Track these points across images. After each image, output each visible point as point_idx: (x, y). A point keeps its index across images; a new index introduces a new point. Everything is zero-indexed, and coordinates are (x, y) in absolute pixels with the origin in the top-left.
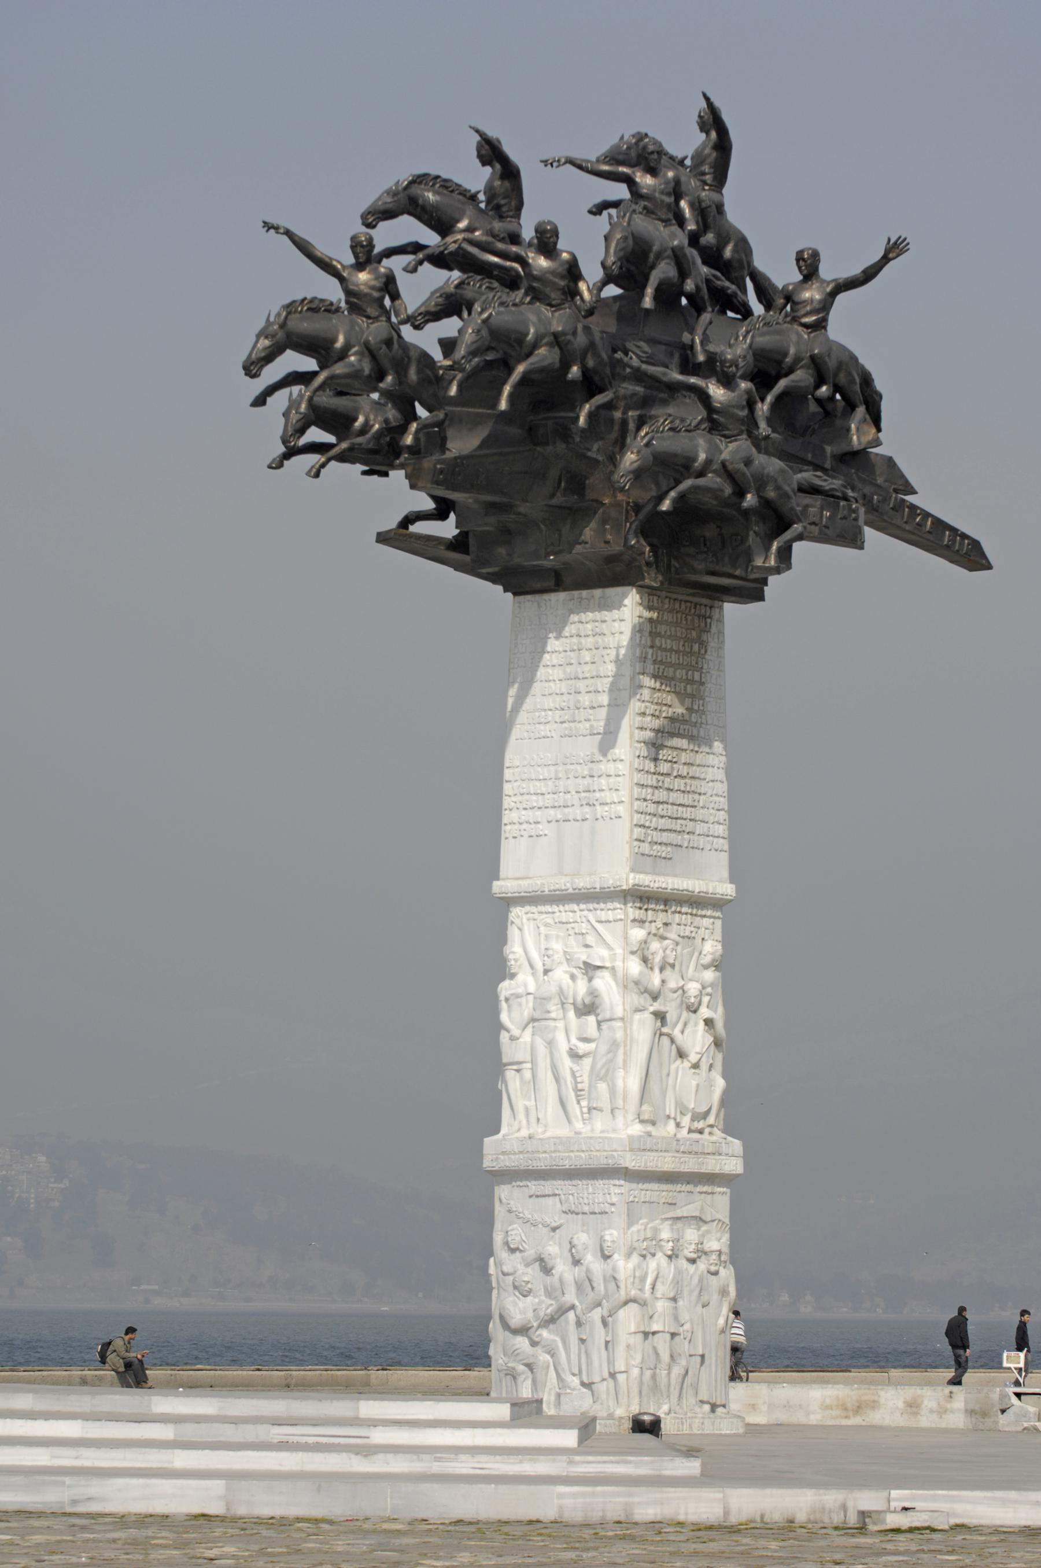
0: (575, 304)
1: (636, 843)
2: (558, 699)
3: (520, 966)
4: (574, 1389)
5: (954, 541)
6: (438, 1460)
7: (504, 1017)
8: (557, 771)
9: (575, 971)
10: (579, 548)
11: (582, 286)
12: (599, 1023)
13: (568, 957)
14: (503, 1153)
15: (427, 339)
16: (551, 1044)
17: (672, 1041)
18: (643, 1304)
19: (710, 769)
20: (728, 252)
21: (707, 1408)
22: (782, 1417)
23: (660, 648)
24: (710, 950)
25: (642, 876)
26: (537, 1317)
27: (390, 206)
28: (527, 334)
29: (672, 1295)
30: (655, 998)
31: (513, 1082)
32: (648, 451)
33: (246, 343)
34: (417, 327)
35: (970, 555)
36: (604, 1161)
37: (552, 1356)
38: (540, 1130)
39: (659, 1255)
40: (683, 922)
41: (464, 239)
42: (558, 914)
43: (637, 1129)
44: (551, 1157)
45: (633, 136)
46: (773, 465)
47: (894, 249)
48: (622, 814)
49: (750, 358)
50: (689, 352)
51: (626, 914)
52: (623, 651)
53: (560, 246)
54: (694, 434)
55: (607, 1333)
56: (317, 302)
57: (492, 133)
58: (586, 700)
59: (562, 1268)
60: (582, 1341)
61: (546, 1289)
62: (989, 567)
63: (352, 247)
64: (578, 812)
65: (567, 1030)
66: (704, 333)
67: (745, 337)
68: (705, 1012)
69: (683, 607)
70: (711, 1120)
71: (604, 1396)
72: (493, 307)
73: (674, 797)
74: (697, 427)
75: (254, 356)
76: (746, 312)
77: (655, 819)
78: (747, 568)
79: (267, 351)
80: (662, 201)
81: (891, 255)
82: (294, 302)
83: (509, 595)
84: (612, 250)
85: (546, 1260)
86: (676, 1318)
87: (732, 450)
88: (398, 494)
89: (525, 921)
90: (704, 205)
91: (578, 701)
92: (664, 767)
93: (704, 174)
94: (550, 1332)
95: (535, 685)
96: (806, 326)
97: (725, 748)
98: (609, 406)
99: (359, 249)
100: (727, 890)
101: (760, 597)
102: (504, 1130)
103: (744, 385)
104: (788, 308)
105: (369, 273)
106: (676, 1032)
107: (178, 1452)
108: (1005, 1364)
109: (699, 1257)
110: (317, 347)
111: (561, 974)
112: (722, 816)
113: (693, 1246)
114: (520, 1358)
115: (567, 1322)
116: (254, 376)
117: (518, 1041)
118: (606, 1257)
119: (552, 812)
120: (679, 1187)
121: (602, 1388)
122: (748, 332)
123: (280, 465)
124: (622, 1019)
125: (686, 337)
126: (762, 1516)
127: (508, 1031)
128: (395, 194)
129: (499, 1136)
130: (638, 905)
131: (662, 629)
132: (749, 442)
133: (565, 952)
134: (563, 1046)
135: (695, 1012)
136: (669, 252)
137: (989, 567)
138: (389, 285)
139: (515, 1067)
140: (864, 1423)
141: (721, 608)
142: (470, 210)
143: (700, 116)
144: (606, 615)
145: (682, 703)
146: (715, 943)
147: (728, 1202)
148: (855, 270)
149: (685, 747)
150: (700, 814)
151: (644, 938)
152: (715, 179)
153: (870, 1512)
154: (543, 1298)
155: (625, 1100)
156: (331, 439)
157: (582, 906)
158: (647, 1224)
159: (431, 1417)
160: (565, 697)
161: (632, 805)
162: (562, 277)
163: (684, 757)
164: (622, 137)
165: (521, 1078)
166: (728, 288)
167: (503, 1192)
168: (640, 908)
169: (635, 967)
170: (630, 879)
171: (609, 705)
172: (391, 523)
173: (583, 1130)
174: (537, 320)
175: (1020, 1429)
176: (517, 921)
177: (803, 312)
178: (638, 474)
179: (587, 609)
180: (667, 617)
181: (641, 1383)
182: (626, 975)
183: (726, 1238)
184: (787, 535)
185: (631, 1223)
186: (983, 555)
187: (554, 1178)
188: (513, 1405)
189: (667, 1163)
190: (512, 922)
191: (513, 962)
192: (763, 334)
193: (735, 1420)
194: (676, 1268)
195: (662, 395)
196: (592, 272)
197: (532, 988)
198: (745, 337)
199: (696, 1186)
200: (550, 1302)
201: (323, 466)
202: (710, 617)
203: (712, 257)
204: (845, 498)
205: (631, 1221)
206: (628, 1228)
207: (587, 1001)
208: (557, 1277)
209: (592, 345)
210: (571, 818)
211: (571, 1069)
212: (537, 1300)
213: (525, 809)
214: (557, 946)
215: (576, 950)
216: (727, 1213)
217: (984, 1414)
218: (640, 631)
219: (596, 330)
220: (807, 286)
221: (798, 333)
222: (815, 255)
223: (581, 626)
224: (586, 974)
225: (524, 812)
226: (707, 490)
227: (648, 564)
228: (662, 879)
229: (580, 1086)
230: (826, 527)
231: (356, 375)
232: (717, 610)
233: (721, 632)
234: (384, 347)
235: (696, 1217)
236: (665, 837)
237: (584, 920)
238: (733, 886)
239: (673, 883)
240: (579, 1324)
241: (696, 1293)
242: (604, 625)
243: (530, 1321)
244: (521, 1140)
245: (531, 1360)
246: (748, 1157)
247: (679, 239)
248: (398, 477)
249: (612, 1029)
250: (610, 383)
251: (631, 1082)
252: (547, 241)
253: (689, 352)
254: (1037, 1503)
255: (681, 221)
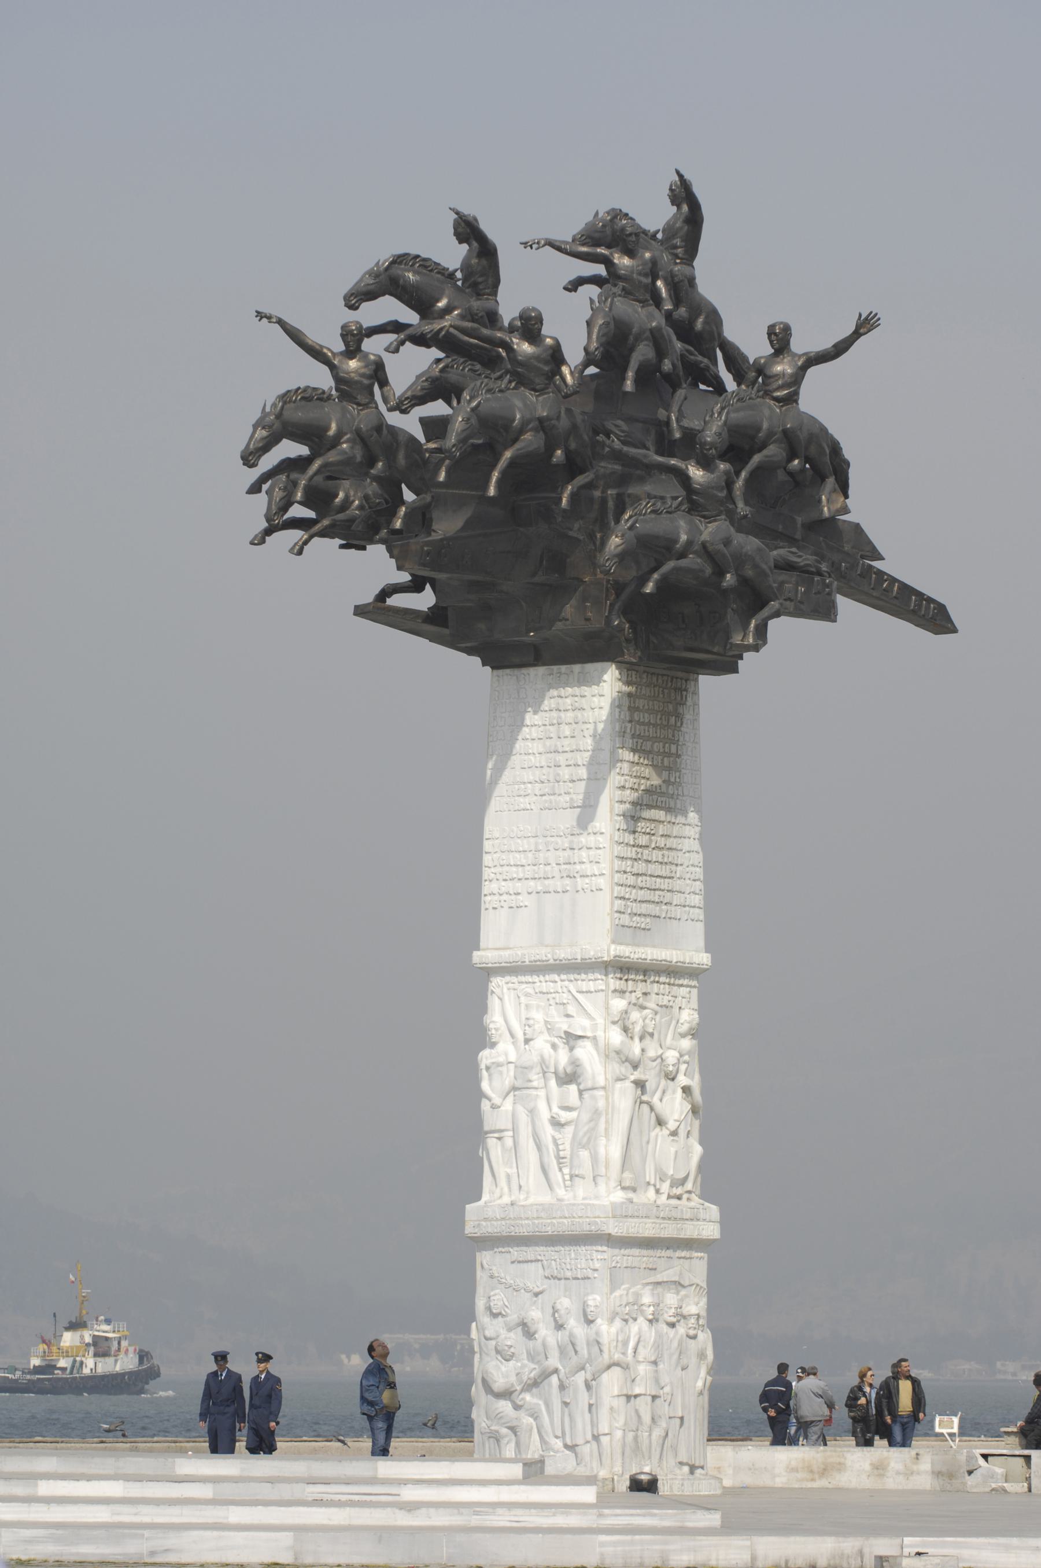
0: (555, 384)
1: (617, 915)
2: (537, 772)
3: (500, 1036)
4: (557, 1452)
5: (920, 606)
6: (476, 1513)
7: (485, 1086)
8: (536, 844)
9: (556, 1040)
10: (559, 625)
11: (565, 370)
12: (581, 1093)
13: (549, 1027)
14: (486, 1219)
15: (410, 423)
16: (532, 1112)
17: (652, 1109)
18: (625, 1367)
19: (687, 840)
20: (699, 324)
21: (686, 1469)
22: (748, 1480)
23: (639, 722)
24: (687, 1018)
25: (622, 947)
26: (520, 1382)
27: (372, 287)
28: (514, 420)
29: (653, 1359)
30: (635, 1067)
31: (495, 1150)
32: (632, 534)
33: (242, 435)
34: (404, 412)
35: (934, 617)
36: (586, 1228)
37: (535, 1419)
38: (522, 1197)
39: (641, 1319)
40: (661, 991)
41: (451, 326)
42: (538, 984)
43: (619, 1196)
44: (533, 1223)
45: (608, 213)
46: (751, 544)
47: (865, 325)
48: (603, 887)
49: (725, 435)
50: (665, 429)
51: (607, 985)
52: (601, 726)
53: (544, 331)
54: (675, 515)
55: (590, 1396)
56: (309, 391)
57: (467, 210)
58: (565, 773)
59: (545, 1332)
60: (566, 1404)
61: (529, 1353)
62: (954, 630)
63: (342, 335)
64: (558, 884)
65: (548, 1099)
66: (680, 410)
67: (720, 414)
68: (682, 1080)
69: (660, 681)
70: (689, 1186)
71: (587, 1458)
72: (481, 395)
73: (653, 869)
74: (677, 508)
75: (251, 446)
76: (719, 388)
77: (634, 891)
78: (725, 646)
79: (265, 442)
80: (640, 282)
81: (862, 331)
82: (289, 391)
83: (488, 669)
84: (594, 337)
85: (529, 1324)
86: (657, 1381)
87: (710, 531)
88: (376, 566)
89: (505, 990)
90: (676, 279)
91: (558, 775)
92: (643, 840)
93: (676, 247)
94: (532, 1396)
95: (513, 758)
96: (777, 400)
97: (701, 819)
98: (590, 486)
99: (349, 338)
100: (703, 959)
101: (735, 670)
102: (485, 1197)
103: (722, 466)
104: (760, 380)
105: (359, 360)
106: (655, 1100)
107: (232, 1508)
108: (938, 1430)
109: (679, 1321)
110: (312, 435)
111: (542, 1044)
112: (698, 886)
113: (673, 1310)
114: (503, 1421)
115: (550, 1385)
116: (251, 466)
117: (499, 1109)
118: (589, 1322)
119: (532, 883)
120: (659, 1253)
121: (585, 1450)
122: (722, 409)
123: (262, 541)
124: (604, 1088)
125: (662, 414)
126: (787, 1562)
127: (490, 1099)
128: (377, 275)
129: (481, 1203)
130: (619, 976)
131: (640, 703)
132: (727, 523)
133: (546, 1022)
134: (544, 1114)
135: (673, 1079)
136: (648, 334)
137: (954, 630)
138: (378, 373)
139: (496, 1135)
140: (830, 1486)
141: (696, 680)
142: (448, 290)
143: (671, 189)
144: (586, 690)
145: (659, 775)
146: (692, 1012)
147: (706, 1266)
148: (825, 343)
149: (662, 819)
150: (677, 884)
151: (625, 1008)
152: (686, 252)
153: (887, 1557)
154: (526, 1362)
155: (607, 1167)
156: (311, 514)
157: (563, 977)
158: (629, 1289)
159: (446, 1476)
160: (545, 770)
161: (613, 877)
162: (546, 363)
163: (661, 829)
164: (597, 214)
165: (503, 1146)
166: (701, 362)
167: (484, 1258)
168: (621, 979)
169: (616, 1037)
170: (612, 951)
171: (588, 779)
172: (368, 597)
173: (566, 1197)
174: (523, 405)
175: (988, 1489)
176: (497, 991)
177: (775, 386)
178: (622, 557)
179: (567, 684)
180: (646, 691)
181: (624, 1445)
182: (607, 1045)
183: (703, 1302)
184: (765, 612)
185: (613, 1288)
186: (949, 619)
187: (537, 1244)
188: (525, 1465)
189: (647, 1229)
190: (493, 992)
191: (493, 1032)
192: (737, 410)
193: (713, 1481)
194: (657, 1332)
195: (639, 472)
196: (574, 354)
197: (512, 1058)
198: (720, 414)
199: (675, 1251)
200: (533, 1366)
201: (306, 543)
202: (686, 690)
203: (684, 331)
204: (819, 573)
205: (614, 1286)
206: (611, 1294)
207: (569, 1070)
208: (539, 1341)
209: (574, 427)
210: (551, 890)
211: (553, 1137)
212: (519, 1364)
213: (505, 880)
214: (538, 1016)
215: (557, 1019)
216: (705, 1278)
217: (951, 1476)
218: (619, 706)
219: (577, 411)
220: (778, 359)
221: (770, 408)
222: (787, 329)
223: (560, 700)
224: (567, 1043)
225: (503, 883)
226: (688, 570)
227: (627, 641)
228: (641, 950)
229: (562, 1154)
230: (801, 602)
231: (348, 462)
232: (693, 683)
233: (696, 704)
234: (375, 434)
235: (675, 1282)
236: (644, 908)
237: (565, 990)
238: (709, 955)
239: (652, 953)
240: (562, 1387)
241: (675, 1357)
242: (584, 699)
243: (513, 1385)
244: (503, 1207)
245: (514, 1424)
246: (724, 1223)
247: (657, 321)
248: (377, 552)
249: (594, 1098)
250: (591, 463)
251: (613, 1149)
252: (530, 325)
253: (665, 429)
254: (1037, 1549)
255: (657, 301)
